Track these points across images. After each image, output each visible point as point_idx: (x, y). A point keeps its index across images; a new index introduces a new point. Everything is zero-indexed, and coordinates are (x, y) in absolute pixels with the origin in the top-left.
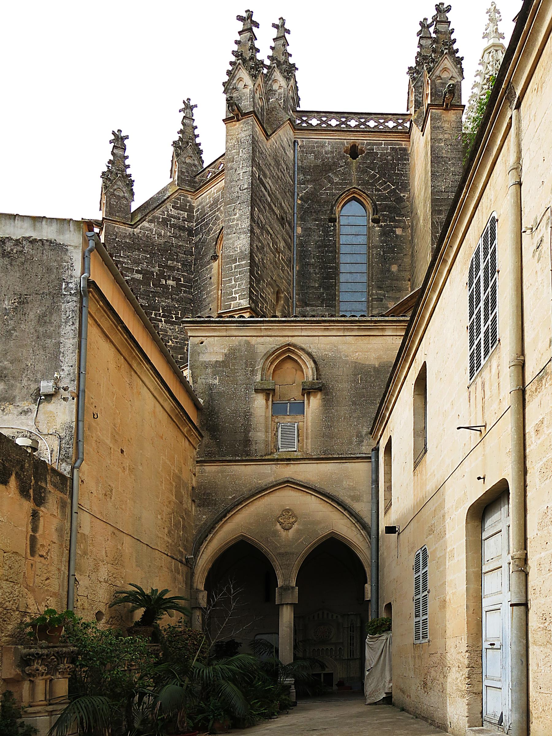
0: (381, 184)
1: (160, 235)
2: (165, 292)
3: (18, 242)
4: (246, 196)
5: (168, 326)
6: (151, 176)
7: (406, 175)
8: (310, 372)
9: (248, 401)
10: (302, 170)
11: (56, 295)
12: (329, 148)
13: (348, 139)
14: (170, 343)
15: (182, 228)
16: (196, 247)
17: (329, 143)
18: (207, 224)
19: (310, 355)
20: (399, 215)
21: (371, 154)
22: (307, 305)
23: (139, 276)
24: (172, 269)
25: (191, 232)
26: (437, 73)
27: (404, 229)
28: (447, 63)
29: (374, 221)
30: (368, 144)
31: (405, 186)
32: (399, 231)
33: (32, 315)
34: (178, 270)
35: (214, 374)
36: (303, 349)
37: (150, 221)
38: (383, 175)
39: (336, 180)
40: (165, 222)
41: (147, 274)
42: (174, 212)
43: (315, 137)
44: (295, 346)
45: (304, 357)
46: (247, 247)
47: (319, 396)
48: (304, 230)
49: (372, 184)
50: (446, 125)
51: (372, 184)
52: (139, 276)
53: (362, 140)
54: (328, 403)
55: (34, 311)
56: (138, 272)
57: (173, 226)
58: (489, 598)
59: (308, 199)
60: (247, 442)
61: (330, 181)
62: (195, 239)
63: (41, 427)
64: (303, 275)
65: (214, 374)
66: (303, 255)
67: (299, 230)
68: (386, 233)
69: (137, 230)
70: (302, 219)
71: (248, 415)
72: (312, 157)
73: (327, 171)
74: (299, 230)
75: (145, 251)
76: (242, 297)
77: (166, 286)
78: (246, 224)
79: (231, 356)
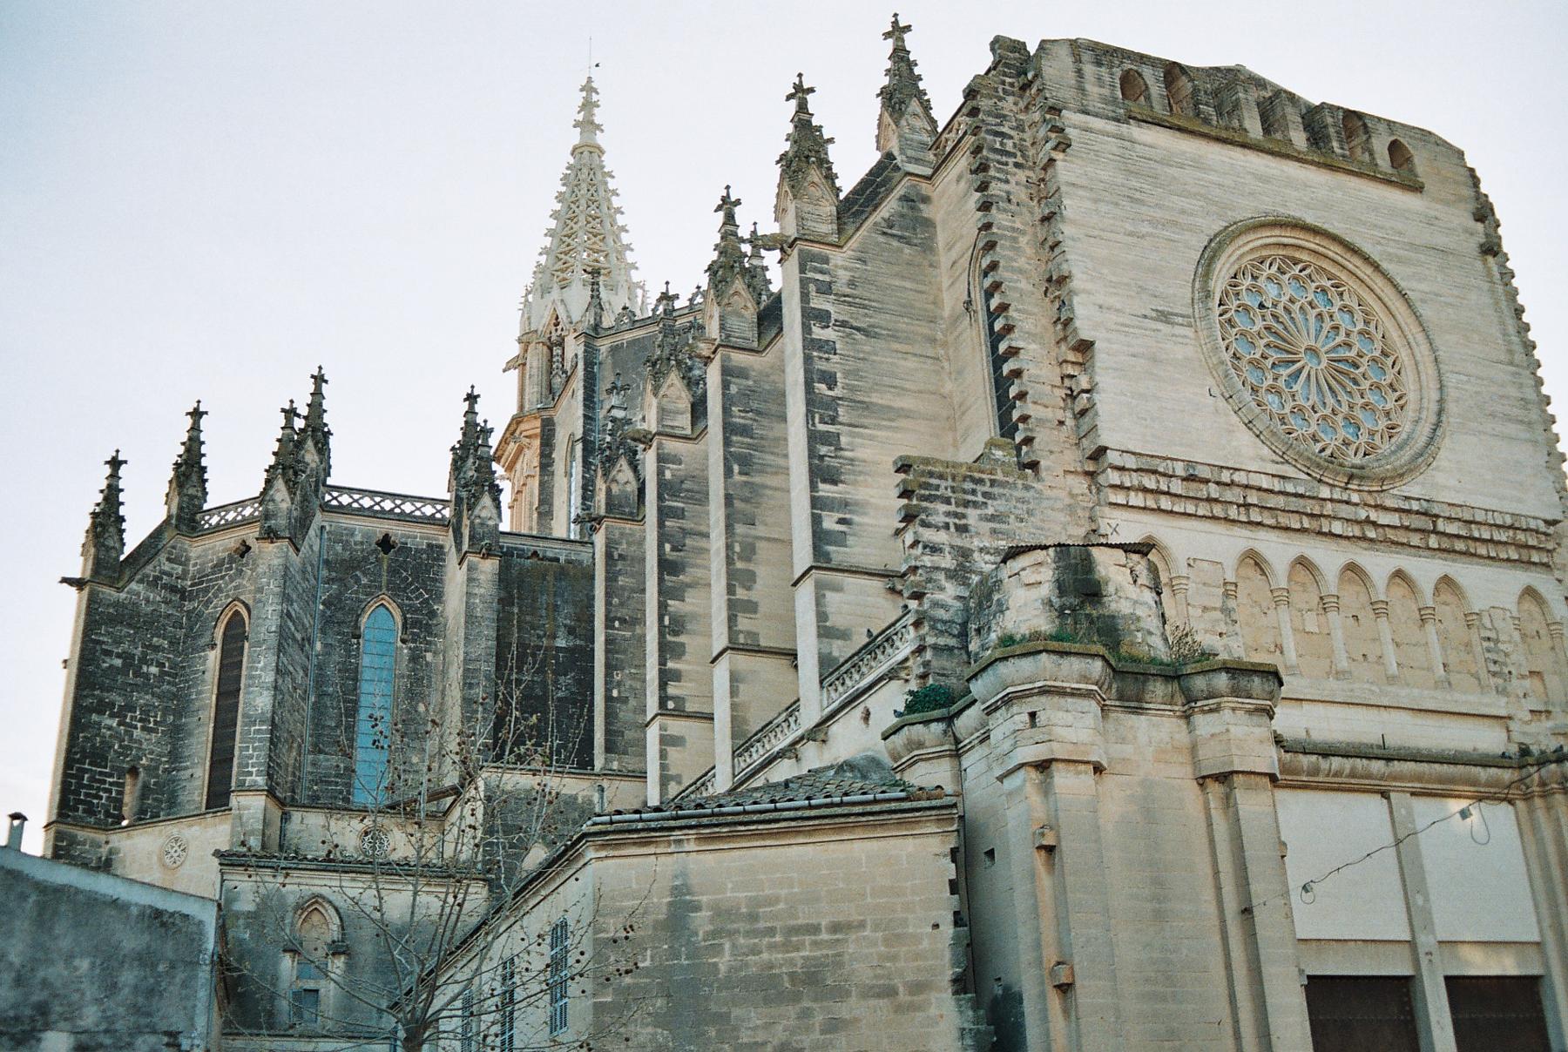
0: (413, 592)
1: (147, 600)
2: (146, 685)
3: (172, 915)
4: (273, 640)
5: (145, 735)
6: (144, 515)
7: (441, 581)
8: (335, 928)
9: (276, 964)
10: (327, 562)
11: (194, 964)
12: (358, 538)
13: (380, 528)
14: (144, 761)
15: (173, 589)
16: (189, 619)
17: (362, 528)
18: (206, 590)
19: (337, 910)
20: (430, 634)
21: (404, 549)
22: (321, 752)
23: (118, 662)
24: (157, 649)
25: (184, 595)
26: (476, 512)
27: (435, 653)
28: (486, 500)
29: (403, 641)
30: (403, 536)
31: (439, 596)
32: (429, 657)
33: (178, 980)
34: (163, 650)
35: (247, 926)
36: (330, 902)
37: (141, 581)
38: (416, 579)
39: (364, 581)
40: (154, 583)
41: (127, 657)
42: (167, 567)
43: (346, 522)
44: (324, 898)
45: (332, 911)
46: (269, 707)
47: (343, 958)
48: (326, 645)
49: (404, 590)
50: (482, 577)
51: (404, 590)
52: (118, 662)
53: (397, 531)
54: (350, 967)
55: (180, 976)
56: (119, 656)
57: (164, 587)
58: (1104, 379)
59: (331, 604)
60: (271, 1014)
61: (358, 581)
62: (188, 606)
63: (145, 1048)
64: (318, 709)
65: (247, 926)
66: (320, 681)
67: (318, 646)
68: (415, 658)
69: (123, 595)
70: (323, 631)
71: (275, 979)
72: (339, 548)
73: (354, 569)
74: (318, 646)
75: (130, 626)
76: (259, 773)
77: (147, 676)
78: (269, 677)
79: (265, 904)
